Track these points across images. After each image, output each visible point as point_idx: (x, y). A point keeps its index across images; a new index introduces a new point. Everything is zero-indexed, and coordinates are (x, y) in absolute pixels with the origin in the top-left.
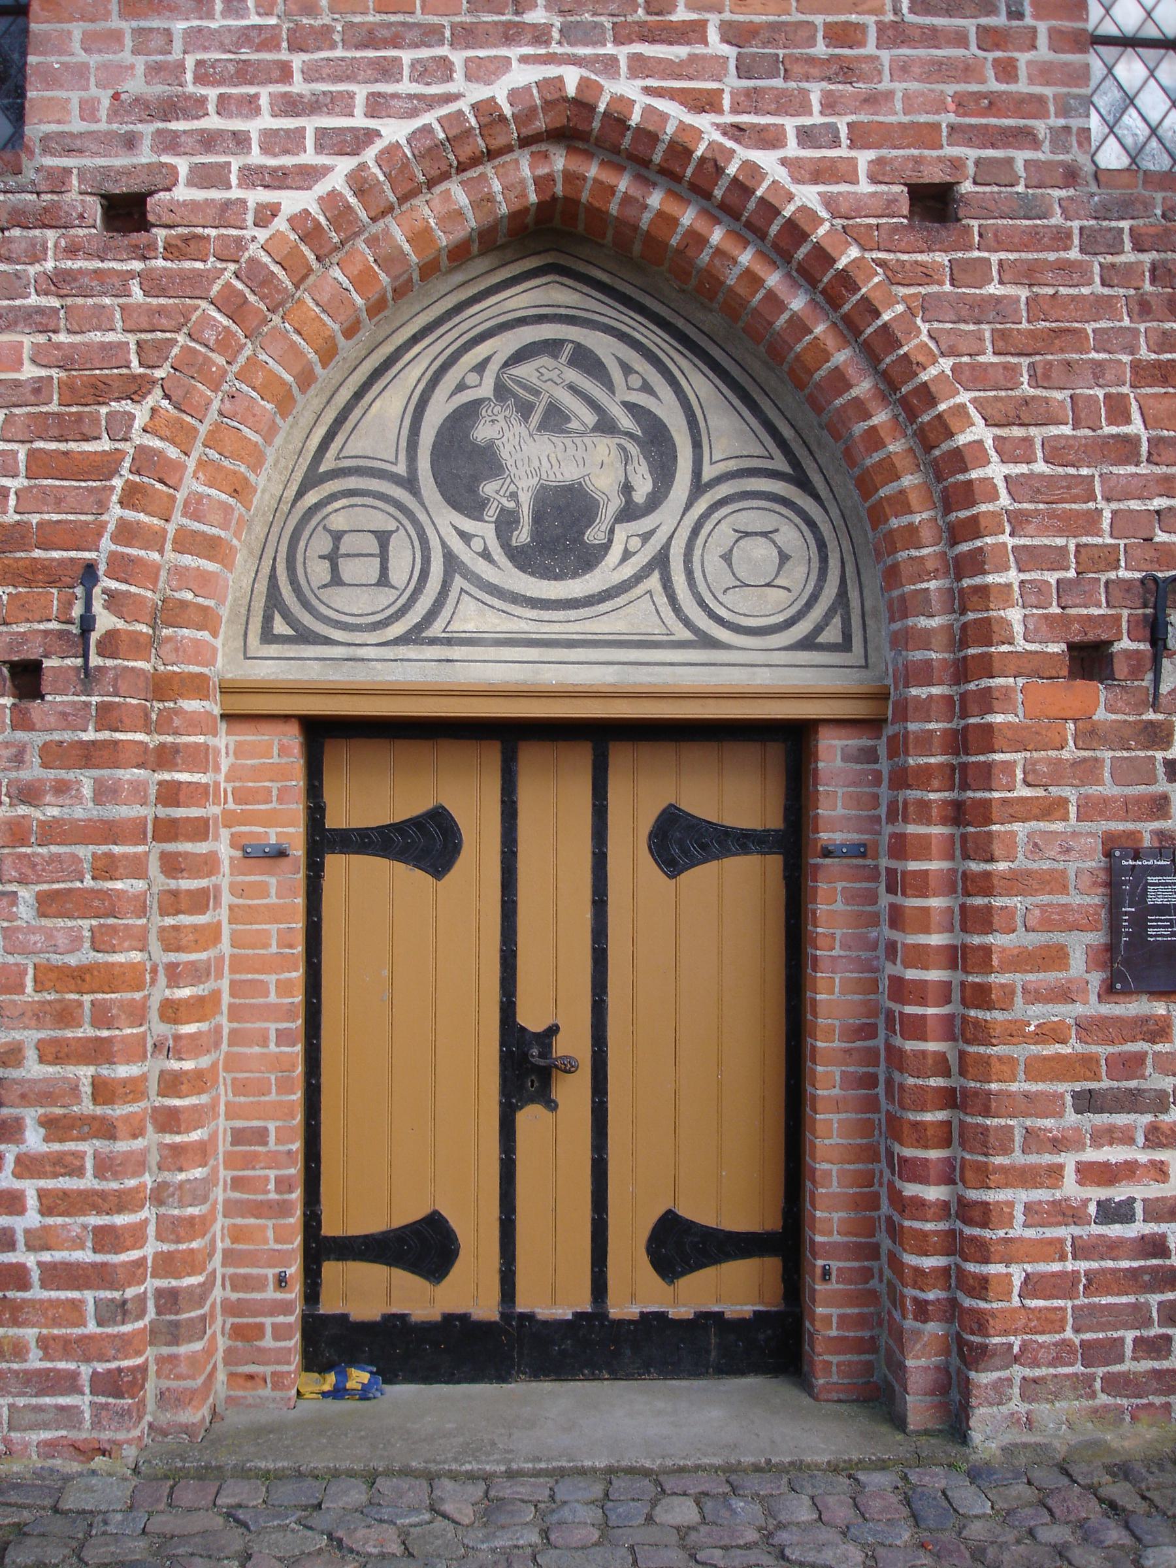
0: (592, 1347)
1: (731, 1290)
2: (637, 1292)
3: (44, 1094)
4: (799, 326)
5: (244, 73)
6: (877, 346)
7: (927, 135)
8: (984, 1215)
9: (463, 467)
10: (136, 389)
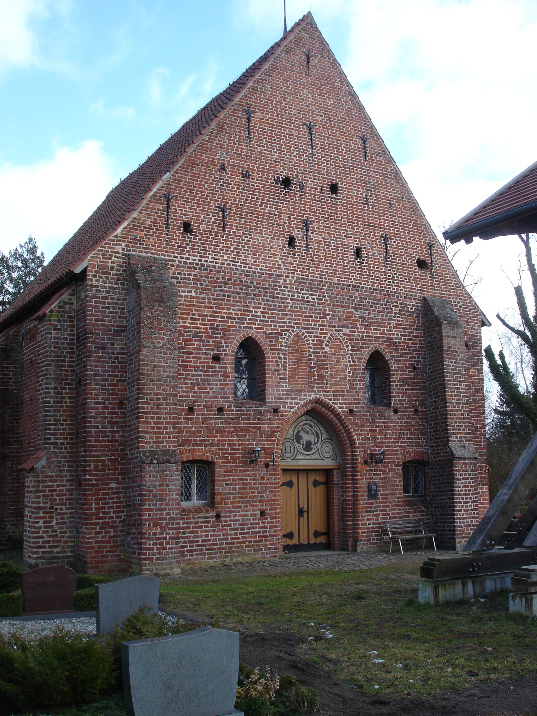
0: (310, 547)
1: (321, 539)
2: (313, 540)
3: (270, 514)
4: (337, 424)
5: (287, 395)
6: (346, 428)
7: (350, 403)
8: (358, 525)
9: (298, 438)
10: (277, 432)
